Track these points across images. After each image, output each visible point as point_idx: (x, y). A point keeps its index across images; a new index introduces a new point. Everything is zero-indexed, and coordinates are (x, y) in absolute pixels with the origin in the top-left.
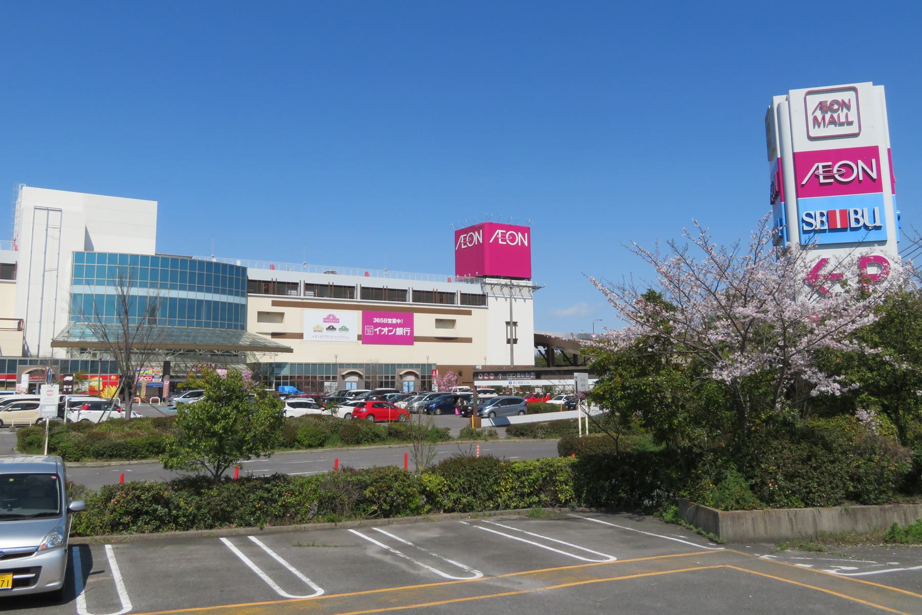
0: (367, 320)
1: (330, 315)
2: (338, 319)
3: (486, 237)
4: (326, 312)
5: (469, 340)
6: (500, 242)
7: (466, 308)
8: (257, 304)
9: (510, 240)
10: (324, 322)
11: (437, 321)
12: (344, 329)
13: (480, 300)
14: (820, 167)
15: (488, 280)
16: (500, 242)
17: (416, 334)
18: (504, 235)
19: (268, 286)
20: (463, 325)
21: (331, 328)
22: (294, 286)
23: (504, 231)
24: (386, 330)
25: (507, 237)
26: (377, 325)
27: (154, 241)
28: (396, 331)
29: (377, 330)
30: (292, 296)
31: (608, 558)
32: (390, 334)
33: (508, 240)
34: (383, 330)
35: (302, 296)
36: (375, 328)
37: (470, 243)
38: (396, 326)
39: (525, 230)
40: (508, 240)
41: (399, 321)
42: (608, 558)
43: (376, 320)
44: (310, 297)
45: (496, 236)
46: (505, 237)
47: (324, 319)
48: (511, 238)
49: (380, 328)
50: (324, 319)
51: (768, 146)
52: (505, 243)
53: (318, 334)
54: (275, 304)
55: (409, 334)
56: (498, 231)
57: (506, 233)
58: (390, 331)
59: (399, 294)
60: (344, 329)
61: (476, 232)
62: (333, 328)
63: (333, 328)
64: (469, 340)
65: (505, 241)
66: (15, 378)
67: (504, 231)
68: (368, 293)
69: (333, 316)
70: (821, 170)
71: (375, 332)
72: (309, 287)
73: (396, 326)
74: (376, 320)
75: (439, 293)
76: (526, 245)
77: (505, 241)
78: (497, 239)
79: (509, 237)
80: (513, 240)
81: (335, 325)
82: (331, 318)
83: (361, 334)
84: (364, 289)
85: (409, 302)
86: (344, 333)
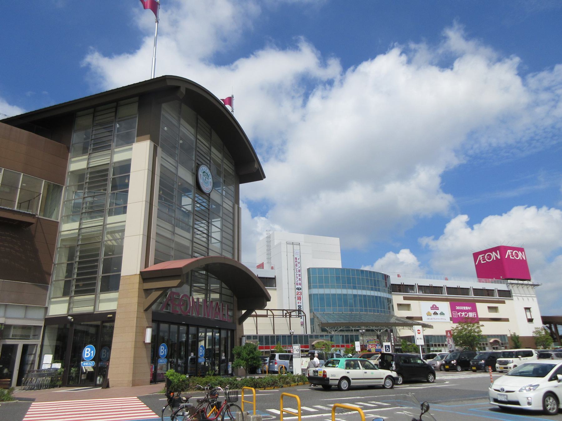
0: (453, 309)
1: (433, 305)
2: (438, 308)
3: (501, 255)
4: (431, 303)
5: (507, 320)
6: (482, 262)
7: (502, 299)
8: (398, 299)
9: (488, 259)
10: (431, 309)
11: (489, 308)
12: (442, 314)
13: (507, 294)
14: (510, 252)
15: (509, 281)
16: (511, 258)
17: (479, 317)
18: (484, 257)
19: (400, 287)
20: (504, 310)
21: (435, 313)
22: (412, 287)
23: (512, 251)
24: (463, 314)
25: (486, 258)
26: (459, 311)
27: (341, 261)
28: (469, 314)
29: (459, 314)
30: (410, 294)
31: (272, 417)
32: (466, 316)
33: (515, 256)
34: (462, 314)
35: (418, 294)
36: (458, 313)
37: (489, 259)
38: (468, 311)
39: (521, 250)
40: (515, 256)
41: (469, 308)
42: (272, 417)
43: (458, 308)
44: (421, 294)
45: (479, 259)
46: (485, 258)
47: (431, 307)
48: (489, 257)
49: (460, 313)
50: (431, 307)
51: (157, 288)
52: (485, 262)
53: (429, 317)
54: (405, 298)
55: (476, 317)
56: (479, 256)
57: (484, 256)
58: (466, 315)
59: (465, 291)
60: (442, 314)
61: (493, 252)
62: (437, 314)
63: (437, 314)
64: (507, 320)
65: (485, 260)
66: (308, 348)
67: (512, 251)
68: (452, 290)
69: (435, 305)
70: (481, 259)
71: (458, 315)
72: (421, 288)
73: (468, 311)
74: (458, 308)
75: (487, 290)
76: (525, 259)
77: (485, 260)
78: (509, 256)
79: (487, 257)
80: (517, 256)
81: (437, 311)
82: (434, 307)
83: (451, 317)
84: (448, 288)
85: (472, 296)
86: (442, 317)
